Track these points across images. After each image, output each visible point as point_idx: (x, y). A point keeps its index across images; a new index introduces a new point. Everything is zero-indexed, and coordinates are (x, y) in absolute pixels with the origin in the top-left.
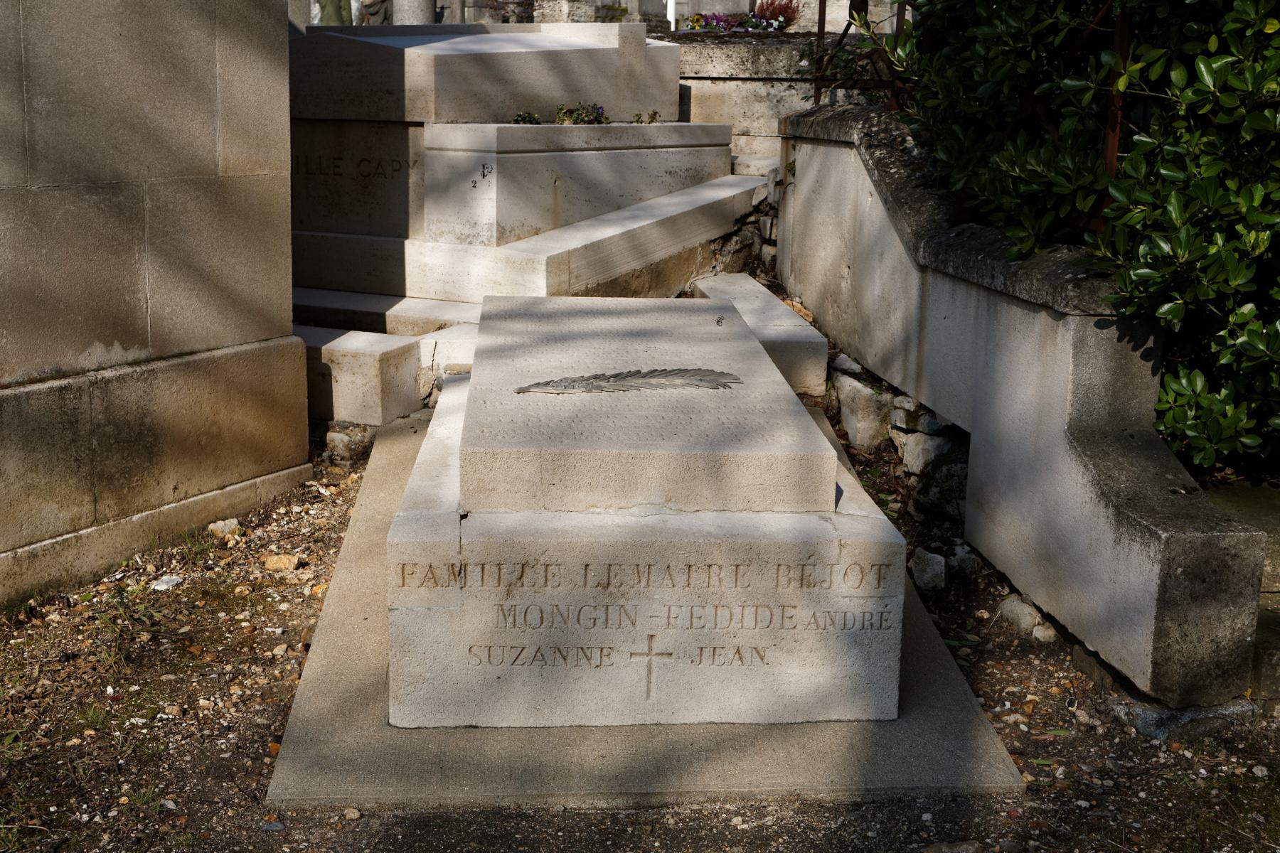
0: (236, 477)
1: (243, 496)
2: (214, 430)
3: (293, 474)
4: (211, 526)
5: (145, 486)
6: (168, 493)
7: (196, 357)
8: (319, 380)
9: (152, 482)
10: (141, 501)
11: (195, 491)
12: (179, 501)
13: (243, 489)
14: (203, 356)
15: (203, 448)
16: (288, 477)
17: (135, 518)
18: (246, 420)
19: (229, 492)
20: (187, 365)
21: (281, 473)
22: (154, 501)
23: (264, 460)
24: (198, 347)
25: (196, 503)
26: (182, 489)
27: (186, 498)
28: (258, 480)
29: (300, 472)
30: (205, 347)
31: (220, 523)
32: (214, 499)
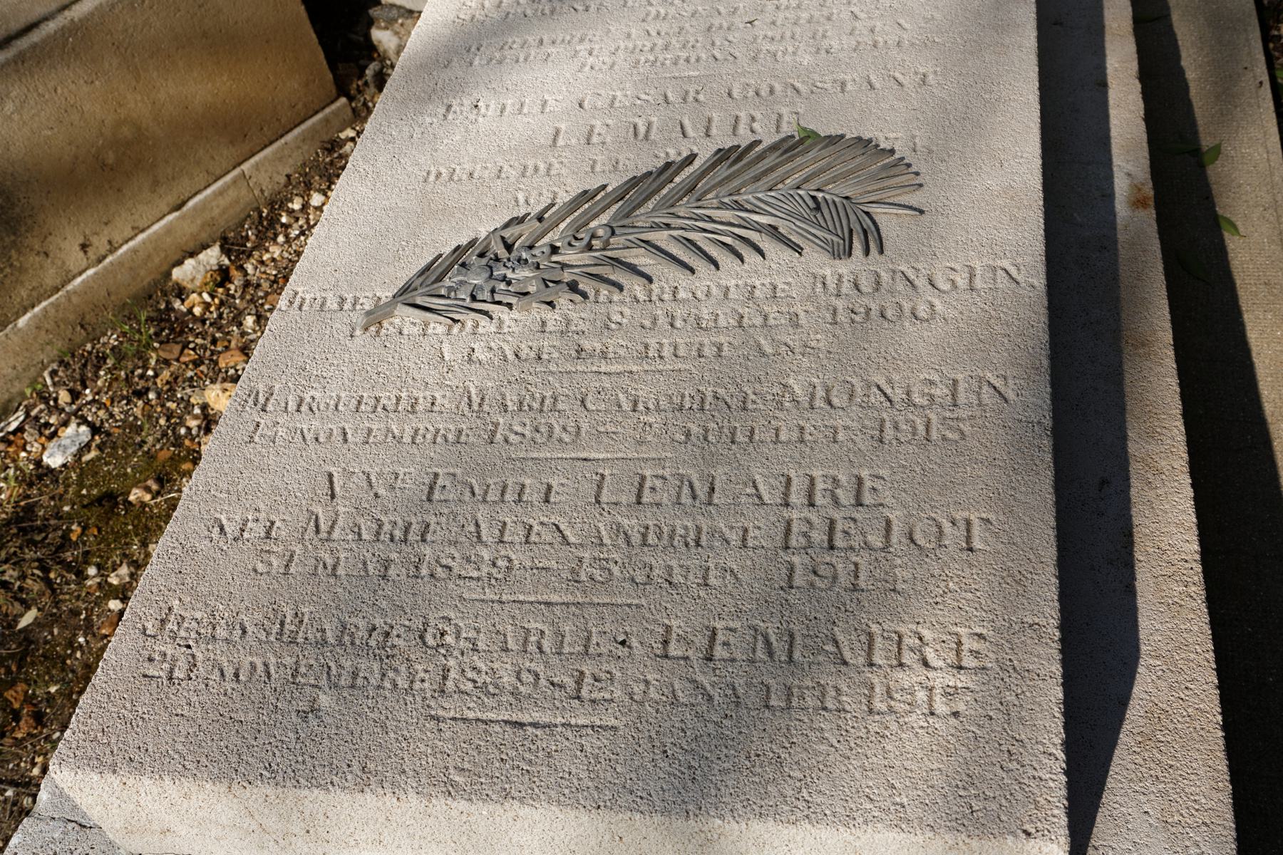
0: (201, 179)
1: (223, 202)
2: (126, 132)
3: (313, 129)
4: (177, 273)
5: (22, 270)
6: (75, 257)
7: (35, 36)
8: (205, 247)
9: (33, 259)
10: (24, 293)
11: (128, 232)
12: (100, 260)
13: (221, 193)
14: (51, 26)
15: (111, 169)
16: (303, 139)
17: (22, 322)
18: (197, 88)
19: (195, 208)
20: (21, 58)
21: (289, 137)
22: (50, 276)
23: (244, 130)
24: (40, 11)
25: (135, 251)
26: (100, 244)
27: (113, 250)
28: (246, 167)
29: (326, 120)
30: (54, 6)
31: (189, 263)
32: (169, 230)
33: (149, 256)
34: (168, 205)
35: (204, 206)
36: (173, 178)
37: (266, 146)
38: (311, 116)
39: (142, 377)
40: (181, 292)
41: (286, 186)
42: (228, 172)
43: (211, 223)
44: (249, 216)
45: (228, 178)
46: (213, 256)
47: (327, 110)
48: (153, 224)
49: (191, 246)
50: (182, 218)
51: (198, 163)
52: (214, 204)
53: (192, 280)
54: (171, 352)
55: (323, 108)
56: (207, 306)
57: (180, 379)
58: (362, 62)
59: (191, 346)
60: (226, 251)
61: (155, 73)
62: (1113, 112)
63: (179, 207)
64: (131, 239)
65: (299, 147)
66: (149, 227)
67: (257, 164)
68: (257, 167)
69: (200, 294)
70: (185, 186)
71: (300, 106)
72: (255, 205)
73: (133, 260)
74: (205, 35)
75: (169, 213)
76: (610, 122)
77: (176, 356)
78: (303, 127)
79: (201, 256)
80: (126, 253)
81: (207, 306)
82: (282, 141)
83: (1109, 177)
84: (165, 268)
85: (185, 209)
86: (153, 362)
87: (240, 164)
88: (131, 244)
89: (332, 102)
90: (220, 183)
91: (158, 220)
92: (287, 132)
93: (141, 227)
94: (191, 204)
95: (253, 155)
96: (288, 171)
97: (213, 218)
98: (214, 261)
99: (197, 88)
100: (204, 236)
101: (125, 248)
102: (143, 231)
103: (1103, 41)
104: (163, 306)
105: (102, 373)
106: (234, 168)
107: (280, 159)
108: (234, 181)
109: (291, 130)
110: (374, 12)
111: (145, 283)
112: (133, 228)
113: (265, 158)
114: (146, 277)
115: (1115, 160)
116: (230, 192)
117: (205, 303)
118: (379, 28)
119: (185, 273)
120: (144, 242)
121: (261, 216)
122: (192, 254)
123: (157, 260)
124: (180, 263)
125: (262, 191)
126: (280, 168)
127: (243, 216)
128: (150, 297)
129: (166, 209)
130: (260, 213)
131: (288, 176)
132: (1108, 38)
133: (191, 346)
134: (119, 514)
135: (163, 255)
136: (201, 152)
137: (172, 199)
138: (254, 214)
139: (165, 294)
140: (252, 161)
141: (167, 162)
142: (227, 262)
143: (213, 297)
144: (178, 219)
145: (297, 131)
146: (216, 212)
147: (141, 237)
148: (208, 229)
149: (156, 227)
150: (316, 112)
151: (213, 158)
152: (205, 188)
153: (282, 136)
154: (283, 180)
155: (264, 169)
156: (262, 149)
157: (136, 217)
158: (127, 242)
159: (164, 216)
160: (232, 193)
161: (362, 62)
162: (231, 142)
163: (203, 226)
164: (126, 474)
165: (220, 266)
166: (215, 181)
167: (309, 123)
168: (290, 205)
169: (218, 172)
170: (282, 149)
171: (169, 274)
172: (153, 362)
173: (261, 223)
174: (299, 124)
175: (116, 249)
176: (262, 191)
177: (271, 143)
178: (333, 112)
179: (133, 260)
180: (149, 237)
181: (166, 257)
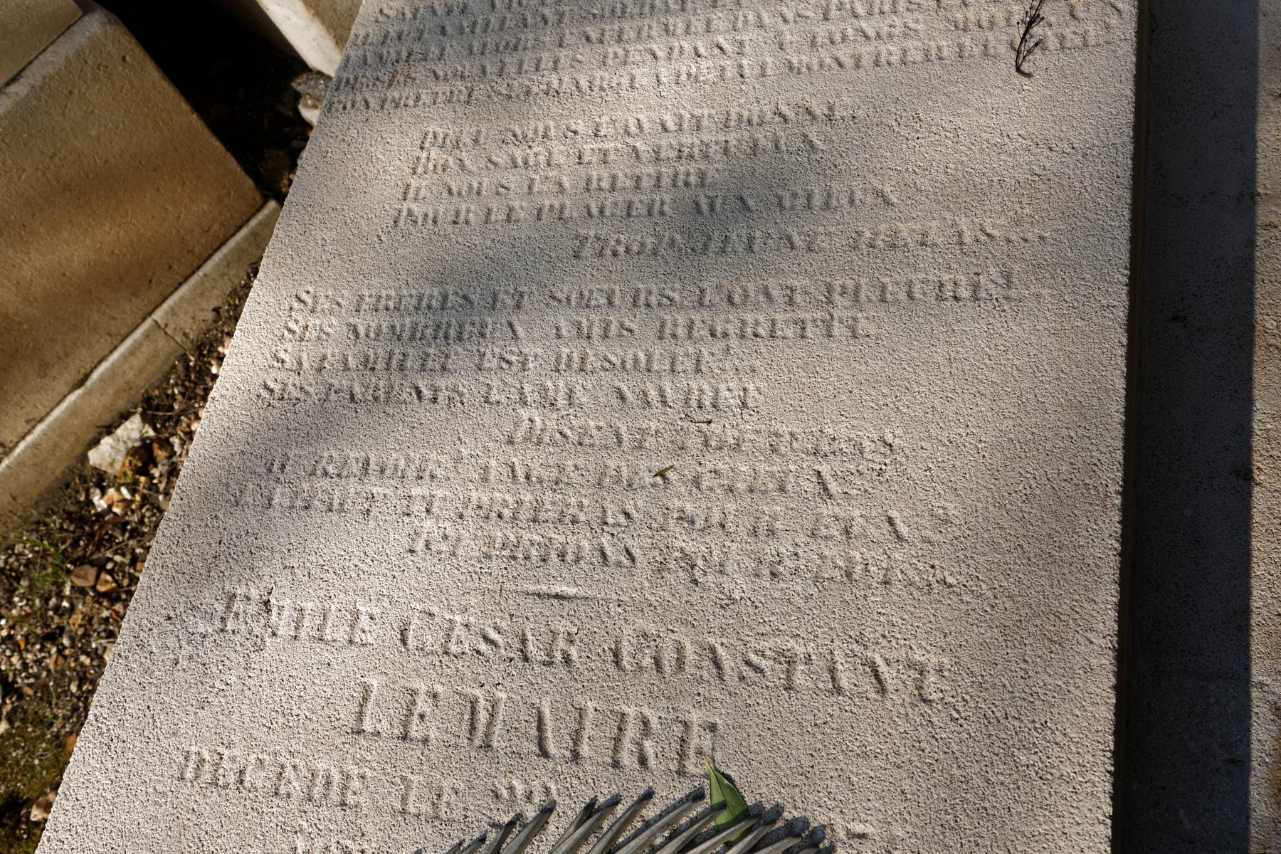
8: (125, 416)
11: (22, 427)
13: (132, 353)
19: (102, 379)
23: (147, 276)
25: (35, 445)
28: (158, 315)
31: (107, 442)
32: (74, 411)
33: (55, 445)
34: (67, 384)
35: (113, 371)
36: (66, 355)
37: (180, 284)
38: (234, 234)
39: (57, 609)
40: (101, 480)
41: (215, 322)
42: (138, 326)
43: (128, 387)
44: (174, 367)
45: (138, 334)
46: (133, 429)
47: (253, 222)
48: (52, 410)
49: (107, 419)
50: (89, 393)
51: (95, 329)
52: (125, 367)
53: (112, 464)
54: (85, 578)
55: (248, 221)
56: (127, 503)
57: (95, 620)
58: (295, 143)
59: (109, 566)
60: (145, 419)
61: (11, 251)
62: (1259, 544)
63: (80, 383)
64: (29, 432)
65: (223, 275)
66: (48, 414)
67: (172, 309)
68: (173, 312)
69: (118, 490)
70: (83, 358)
71: (216, 227)
72: (181, 351)
73: (35, 456)
74: (67, 187)
75: (70, 392)
76: (439, 689)
77: (92, 583)
78: (225, 250)
79: (120, 432)
80: (24, 451)
81: (127, 503)
82: (201, 273)
83: (1243, 715)
84: (79, 450)
85: (88, 383)
86: (67, 591)
87: (150, 314)
88: (29, 439)
89: (259, 210)
90: (128, 343)
91: (58, 404)
92: (205, 261)
93: (38, 416)
94: (95, 375)
95: (166, 299)
96: (215, 304)
97: (128, 383)
98: (136, 435)
99: (74, 248)
100: (121, 404)
101: (22, 445)
102: (41, 420)
103: (1250, 363)
104: (82, 498)
105: (16, 599)
106: (144, 319)
107: (202, 295)
108: (147, 336)
109: (210, 256)
110: (299, 85)
111: (58, 473)
112: (27, 422)
113: (181, 299)
114: (57, 468)
115: (1255, 669)
116: (144, 348)
117: (124, 500)
118: (306, 106)
119: (103, 455)
120: (45, 433)
121: (187, 367)
122: (109, 430)
123: (66, 447)
124: (95, 442)
125: (186, 335)
126: (204, 305)
127: (166, 368)
128: (68, 486)
129: (66, 390)
130: (187, 361)
131: (217, 310)
132: (1259, 355)
133: (109, 566)
134: (20, 839)
135: (72, 439)
136: (96, 316)
137: (70, 377)
138: (180, 367)
139: (84, 480)
140: (166, 306)
141: (52, 340)
142: (151, 433)
143: (133, 492)
144: (82, 396)
145: (217, 257)
146: (131, 374)
147: (40, 428)
148: (125, 396)
149: (56, 413)
150: (240, 228)
151: (114, 318)
152: (111, 352)
153: (199, 267)
154: (210, 316)
155: (180, 311)
156: (176, 289)
157: (28, 409)
158: (23, 438)
159: (65, 396)
160: (147, 349)
161: (295, 143)
162: (133, 294)
163: (117, 394)
164: (33, 767)
165: (143, 439)
166: (122, 341)
167: (232, 243)
168: (220, 349)
169: (123, 331)
170: (202, 282)
171: (84, 458)
172: (67, 591)
173: (188, 376)
174: (219, 248)
175: (12, 449)
176: (186, 335)
177: (186, 279)
178: (260, 223)
179: (35, 456)
180: (50, 427)
181: (77, 440)
